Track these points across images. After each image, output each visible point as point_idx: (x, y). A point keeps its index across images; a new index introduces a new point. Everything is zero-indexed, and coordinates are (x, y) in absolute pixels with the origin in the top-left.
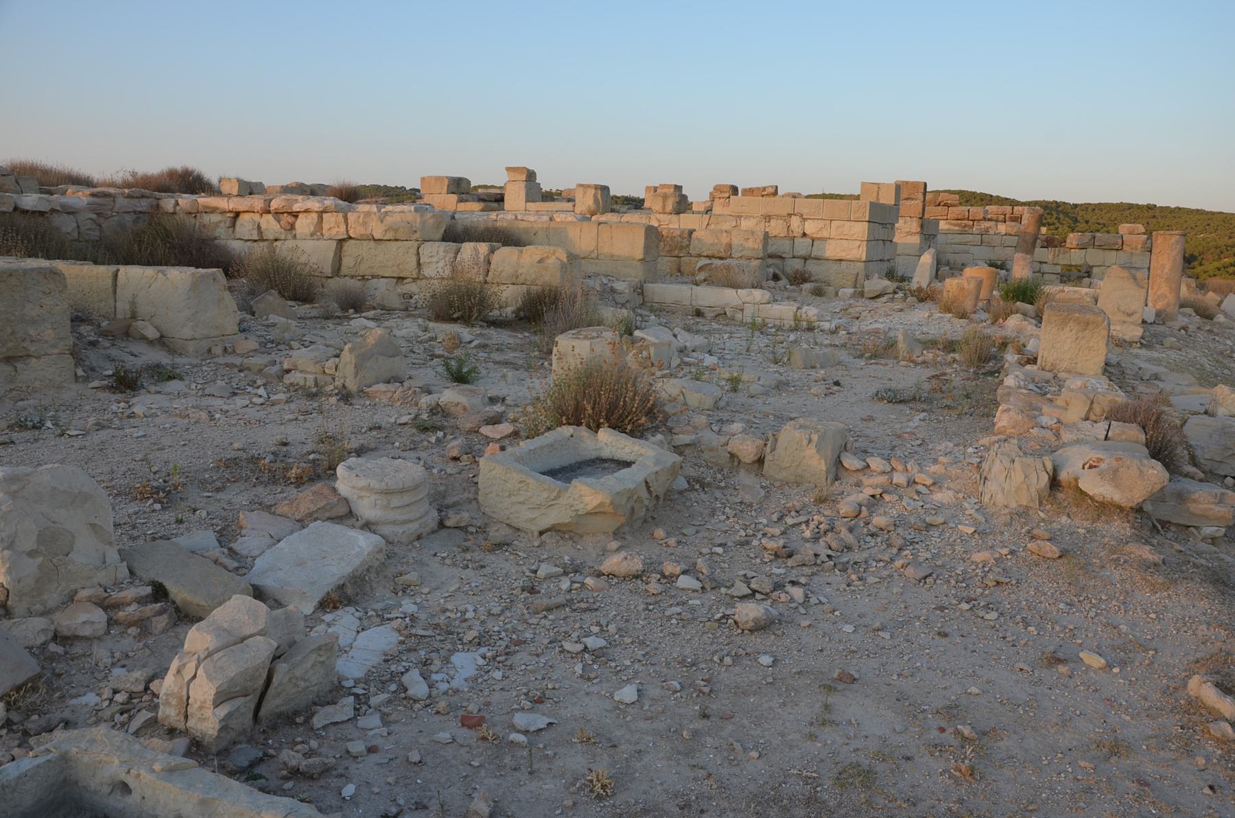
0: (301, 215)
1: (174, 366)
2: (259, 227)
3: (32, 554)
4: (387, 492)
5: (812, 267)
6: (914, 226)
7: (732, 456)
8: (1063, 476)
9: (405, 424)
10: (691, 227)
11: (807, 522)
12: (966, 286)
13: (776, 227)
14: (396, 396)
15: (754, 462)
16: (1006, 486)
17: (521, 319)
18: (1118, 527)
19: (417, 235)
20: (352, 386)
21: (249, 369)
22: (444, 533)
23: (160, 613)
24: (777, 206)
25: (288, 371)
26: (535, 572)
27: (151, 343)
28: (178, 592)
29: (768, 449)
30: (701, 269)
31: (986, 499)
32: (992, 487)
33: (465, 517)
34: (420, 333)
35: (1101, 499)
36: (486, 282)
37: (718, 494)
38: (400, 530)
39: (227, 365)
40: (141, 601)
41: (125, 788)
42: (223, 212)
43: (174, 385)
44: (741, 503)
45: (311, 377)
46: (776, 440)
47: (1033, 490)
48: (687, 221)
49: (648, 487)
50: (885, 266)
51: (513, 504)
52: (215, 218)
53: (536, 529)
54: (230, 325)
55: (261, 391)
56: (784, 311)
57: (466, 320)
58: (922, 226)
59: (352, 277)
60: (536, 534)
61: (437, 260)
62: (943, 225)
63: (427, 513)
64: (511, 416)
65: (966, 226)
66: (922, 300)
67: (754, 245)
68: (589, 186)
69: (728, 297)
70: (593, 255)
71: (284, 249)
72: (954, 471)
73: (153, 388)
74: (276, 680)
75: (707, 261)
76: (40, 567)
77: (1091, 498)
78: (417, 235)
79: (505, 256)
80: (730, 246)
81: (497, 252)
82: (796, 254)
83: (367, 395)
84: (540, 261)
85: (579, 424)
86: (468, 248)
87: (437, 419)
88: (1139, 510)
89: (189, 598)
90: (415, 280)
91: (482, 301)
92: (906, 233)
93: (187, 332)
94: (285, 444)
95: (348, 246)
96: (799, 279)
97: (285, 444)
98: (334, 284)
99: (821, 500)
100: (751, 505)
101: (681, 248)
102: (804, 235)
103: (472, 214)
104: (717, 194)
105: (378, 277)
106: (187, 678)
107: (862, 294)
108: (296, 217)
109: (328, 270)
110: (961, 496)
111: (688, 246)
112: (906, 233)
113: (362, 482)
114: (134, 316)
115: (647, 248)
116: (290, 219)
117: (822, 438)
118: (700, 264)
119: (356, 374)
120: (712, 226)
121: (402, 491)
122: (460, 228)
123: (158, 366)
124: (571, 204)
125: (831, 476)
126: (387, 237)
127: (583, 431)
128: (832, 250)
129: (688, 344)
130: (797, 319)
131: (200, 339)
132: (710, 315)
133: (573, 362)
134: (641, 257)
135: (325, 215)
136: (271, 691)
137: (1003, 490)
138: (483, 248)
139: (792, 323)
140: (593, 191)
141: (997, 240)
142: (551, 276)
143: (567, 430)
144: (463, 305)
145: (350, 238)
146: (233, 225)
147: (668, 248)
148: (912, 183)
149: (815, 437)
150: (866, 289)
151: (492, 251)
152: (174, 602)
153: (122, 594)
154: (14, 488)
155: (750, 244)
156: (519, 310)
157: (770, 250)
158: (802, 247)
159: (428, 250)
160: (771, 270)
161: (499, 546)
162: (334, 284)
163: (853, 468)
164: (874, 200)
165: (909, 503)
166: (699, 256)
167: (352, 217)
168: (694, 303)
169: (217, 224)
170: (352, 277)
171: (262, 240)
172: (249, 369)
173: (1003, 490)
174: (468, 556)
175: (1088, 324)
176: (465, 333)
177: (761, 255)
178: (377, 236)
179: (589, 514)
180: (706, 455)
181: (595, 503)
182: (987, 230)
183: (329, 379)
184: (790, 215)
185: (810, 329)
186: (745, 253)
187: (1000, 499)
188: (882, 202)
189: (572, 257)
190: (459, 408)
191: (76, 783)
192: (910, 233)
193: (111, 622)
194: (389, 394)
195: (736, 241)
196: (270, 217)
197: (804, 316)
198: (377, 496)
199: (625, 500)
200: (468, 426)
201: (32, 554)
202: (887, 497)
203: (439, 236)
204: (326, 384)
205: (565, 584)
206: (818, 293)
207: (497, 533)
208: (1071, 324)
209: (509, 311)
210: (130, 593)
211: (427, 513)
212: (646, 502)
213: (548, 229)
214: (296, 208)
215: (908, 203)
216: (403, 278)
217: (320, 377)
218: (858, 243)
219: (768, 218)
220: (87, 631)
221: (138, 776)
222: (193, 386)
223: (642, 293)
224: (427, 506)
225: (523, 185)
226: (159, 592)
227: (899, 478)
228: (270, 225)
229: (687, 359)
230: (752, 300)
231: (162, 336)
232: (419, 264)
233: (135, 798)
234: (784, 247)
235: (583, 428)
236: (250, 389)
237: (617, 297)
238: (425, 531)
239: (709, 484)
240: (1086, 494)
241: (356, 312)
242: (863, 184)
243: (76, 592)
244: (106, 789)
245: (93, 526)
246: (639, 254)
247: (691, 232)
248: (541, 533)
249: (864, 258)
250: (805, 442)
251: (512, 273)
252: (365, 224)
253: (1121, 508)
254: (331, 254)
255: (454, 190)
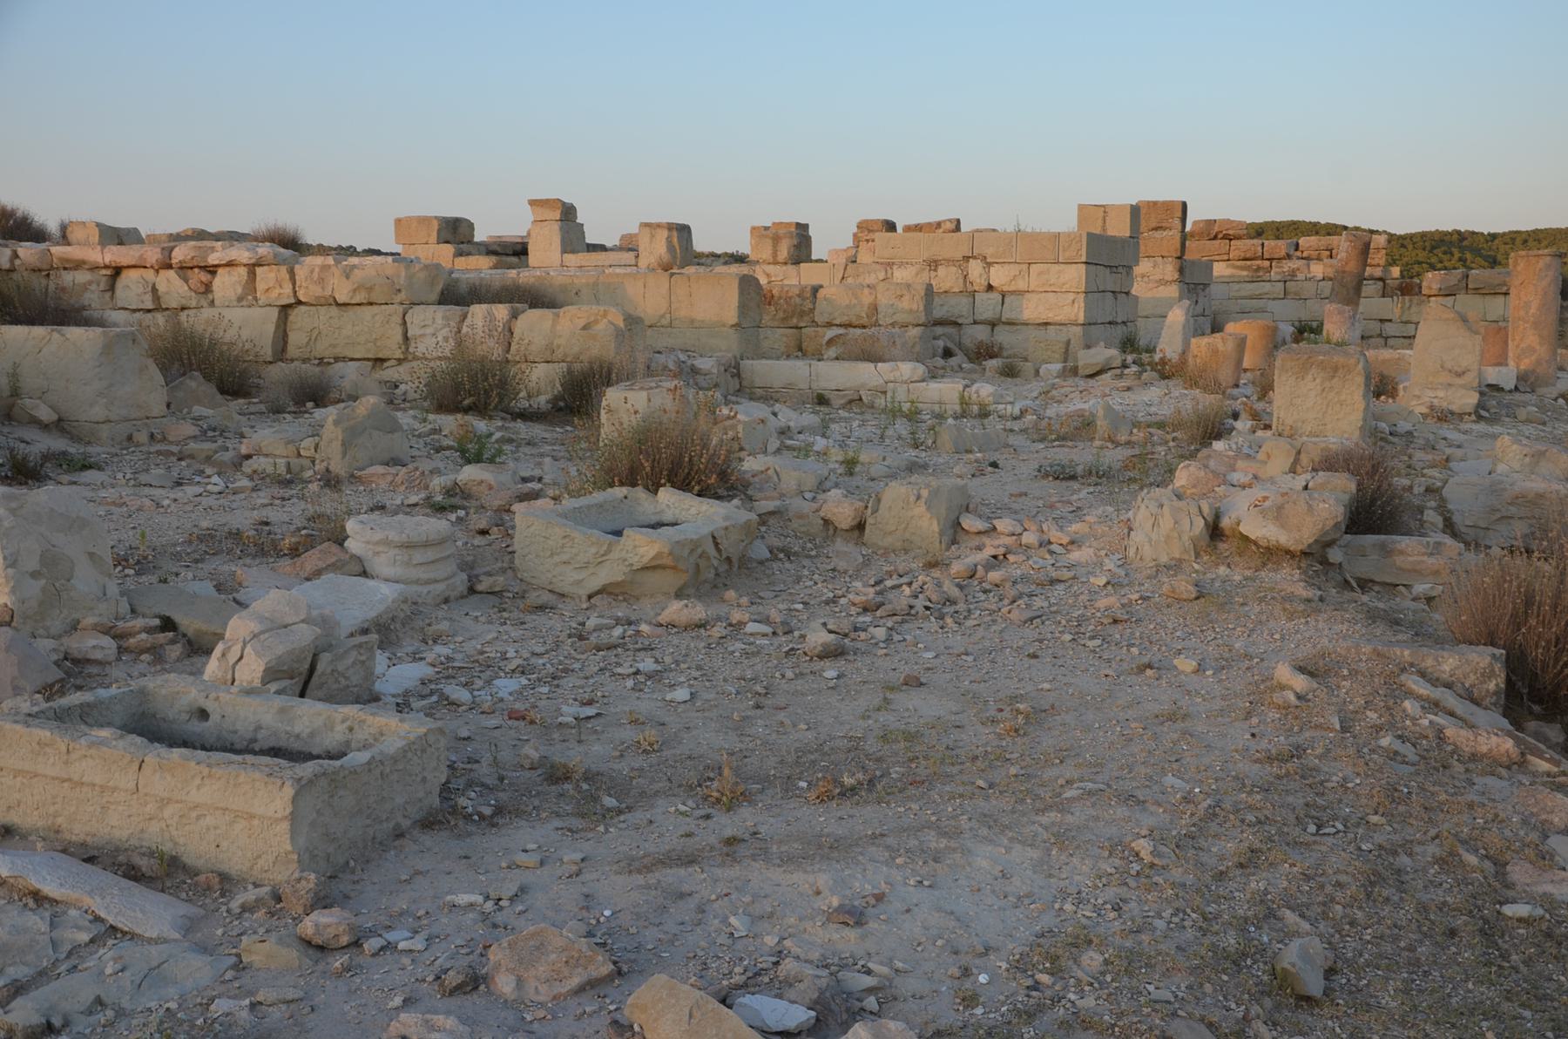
0: (220, 271)
1: (86, 456)
2: (154, 290)
3: (35, 575)
4: (408, 546)
5: (1003, 336)
6: (1169, 270)
7: (826, 522)
8: (1225, 523)
9: (415, 505)
10: (815, 282)
11: (910, 584)
12: (1221, 347)
13: (947, 279)
14: (398, 479)
15: (852, 529)
16: (1154, 537)
17: (560, 409)
18: (1289, 579)
19: (402, 296)
20: (338, 467)
21: (192, 457)
22: (475, 598)
23: (173, 642)
24: (951, 248)
25: (248, 457)
26: (583, 624)
27: (45, 427)
28: (189, 622)
29: (869, 511)
30: (830, 342)
31: (1131, 552)
32: (1137, 537)
33: (500, 581)
34: (417, 425)
35: (1263, 543)
36: (508, 361)
37: (806, 562)
38: (424, 589)
39: (159, 453)
40: (150, 630)
41: (203, 714)
42: (95, 268)
43: (90, 475)
44: (834, 570)
45: (281, 462)
46: (879, 500)
47: (1185, 538)
48: (809, 274)
49: (716, 544)
50: (1119, 332)
51: (556, 565)
52: (82, 277)
53: (584, 593)
54: (158, 408)
55: (215, 479)
56: (946, 391)
57: (480, 409)
58: (1181, 271)
59: (305, 361)
60: (584, 598)
61: (434, 331)
62: (1219, 269)
63: (454, 575)
64: (551, 493)
65: (1259, 268)
66: (1164, 377)
67: (912, 305)
68: (659, 226)
69: (864, 374)
70: (665, 322)
71: (199, 320)
72: (1100, 529)
73: (65, 478)
74: (320, 667)
75: (841, 331)
76: (44, 590)
77: (1255, 543)
78: (402, 296)
79: (534, 326)
80: (875, 308)
81: (522, 318)
82: (978, 317)
83: (359, 480)
84: (584, 328)
85: (634, 485)
86: (478, 311)
87: (456, 501)
88: (1305, 554)
89: (204, 627)
90: (400, 361)
91: (503, 383)
92: (1153, 280)
93: (98, 412)
94: (267, 524)
95: (297, 315)
96: (983, 353)
97: (267, 524)
98: (277, 371)
99: (932, 565)
100: (845, 572)
101: (802, 314)
102: (990, 288)
103: (478, 268)
104: (864, 235)
105: (344, 359)
106: (232, 661)
107: (1074, 371)
108: (213, 273)
109: (268, 352)
110: (1103, 553)
111: (812, 310)
112: (1153, 280)
113: (378, 536)
114: (15, 392)
115: (743, 308)
116: (205, 277)
117: (935, 493)
118: (831, 333)
119: (344, 454)
120: (850, 280)
121: (426, 545)
122: (463, 288)
123: (64, 453)
124: (632, 254)
125: (946, 539)
126: (357, 300)
127: (640, 492)
128: (1032, 309)
129: (792, 424)
130: (964, 402)
131: (117, 422)
132: (837, 402)
133: (629, 421)
134: (734, 320)
135: (259, 270)
136: (315, 679)
137: (1150, 540)
138: (501, 311)
139: (958, 408)
140: (665, 233)
141: (1310, 289)
142: (602, 347)
143: (619, 492)
144: (475, 391)
145: (299, 303)
146: (112, 288)
147: (781, 314)
148: (1164, 203)
149: (925, 493)
150: (1080, 363)
151: (515, 315)
152: (184, 635)
153: (130, 624)
154: (14, 505)
155: (905, 304)
156: (556, 399)
157: (938, 313)
158: (987, 306)
159: (417, 316)
160: (941, 343)
161: (541, 608)
162: (277, 371)
163: (974, 529)
164: (1098, 231)
165: (1041, 560)
166: (829, 325)
167: (301, 272)
168: (814, 386)
169: (85, 287)
170: (305, 361)
171: (158, 308)
172: (192, 457)
173: (1150, 540)
174: (505, 614)
175: (1336, 369)
176: (481, 425)
177: (923, 320)
178: (341, 298)
179: (645, 568)
180: (795, 524)
181: (652, 553)
182: (1293, 274)
183: (307, 463)
184: (967, 259)
185: (984, 414)
186: (899, 318)
187: (1147, 551)
188: (1110, 233)
189: (632, 321)
190: (483, 488)
191: (154, 716)
192: (1163, 282)
193: (121, 650)
194: (390, 478)
195: (884, 300)
196: (171, 273)
197: (974, 396)
198: (397, 551)
199: (686, 552)
200: (497, 503)
201: (35, 575)
202: (1011, 558)
203: (434, 296)
204: (302, 469)
205: (618, 631)
206: (1010, 372)
207: (534, 598)
208: (1313, 370)
209: (542, 401)
210: (139, 623)
211: (454, 575)
212: (715, 563)
213: (596, 284)
214: (213, 259)
215: (1158, 234)
216: (382, 360)
217: (294, 461)
218: (1071, 296)
219: (933, 264)
220: (98, 655)
221: (217, 699)
222: (120, 476)
223: (738, 375)
224: (454, 567)
225: (556, 226)
226: (168, 624)
227: (1030, 538)
228: (172, 286)
229: (789, 442)
230: (900, 376)
231: (60, 420)
232: (406, 338)
233: (215, 718)
234: (958, 307)
235: (640, 489)
236: (198, 479)
237: (700, 379)
238: (453, 594)
239: (795, 554)
240: (1247, 539)
241: (317, 406)
242: (1081, 207)
243: (78, 622)
244: (185, 717)
245: (91, 555)
246: (731, 316)
247: (816, 290)
248: (590, 597)
249: (1081, 319)
250: (912, 499)
251: (545, 343)
252: (321, 281)
253: (1288, 552)
254: (270, 328)
255: (450, 237)
